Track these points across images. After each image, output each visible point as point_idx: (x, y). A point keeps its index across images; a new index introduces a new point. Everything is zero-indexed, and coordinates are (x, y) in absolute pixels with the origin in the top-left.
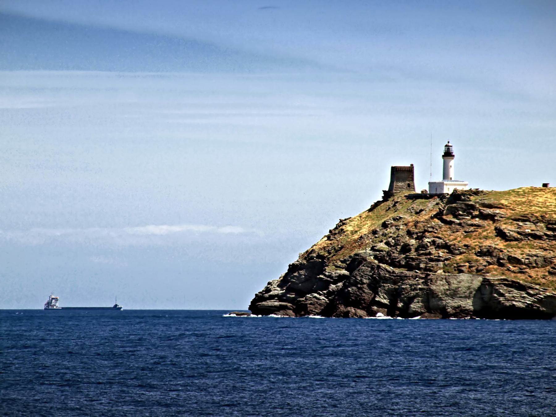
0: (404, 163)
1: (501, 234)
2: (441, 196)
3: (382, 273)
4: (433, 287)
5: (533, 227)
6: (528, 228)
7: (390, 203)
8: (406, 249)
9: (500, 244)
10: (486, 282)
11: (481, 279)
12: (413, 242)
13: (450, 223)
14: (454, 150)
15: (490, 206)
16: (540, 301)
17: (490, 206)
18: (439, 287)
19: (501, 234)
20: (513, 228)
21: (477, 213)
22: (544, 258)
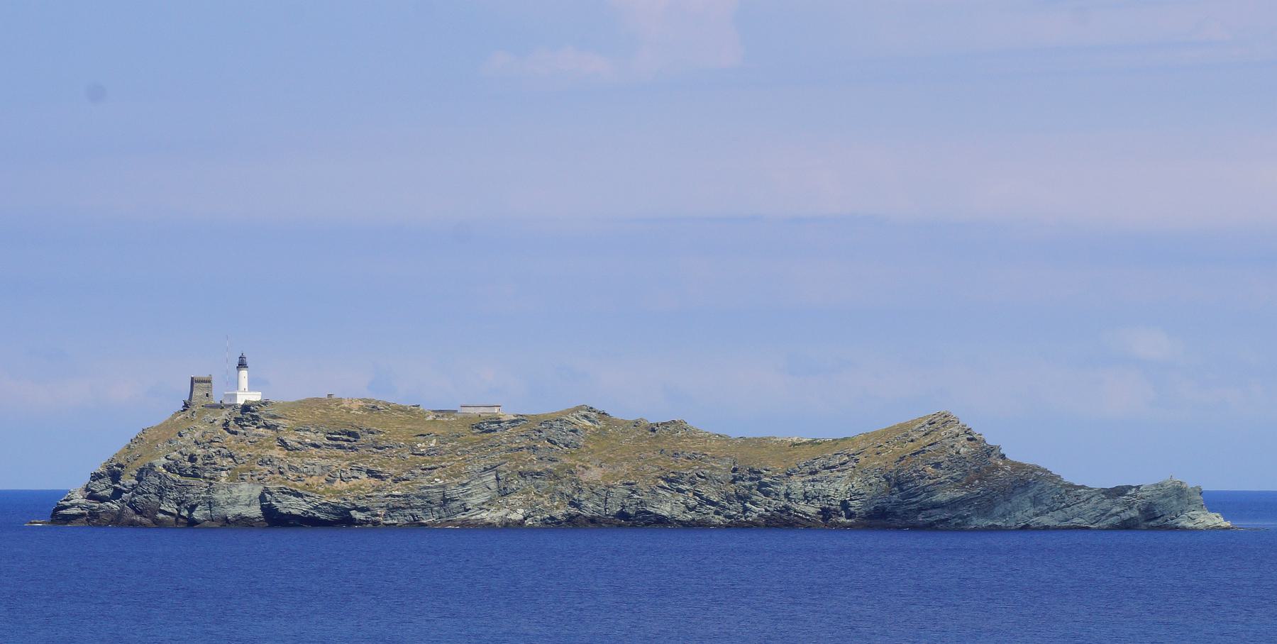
0: (203, 375)
1: (284, 444)
2: (235, 406)
3: (168, 483)
4: (215, 496)
5: (313, 436)
6: (310, 437)
7: (188, 412)
8: (192, 458)
9: (277, 453)
10: (266, 490)
11: (261, 487)
12: (199, 451)
13: (236, 433)
14: (248, 361)
15: (274, 417)
16: (316, 508)
17: (274, 417)
18: (220, 496)
19: (284, 444)
20: (294, 438)
21: (262, 423)
22: (899, 484)
